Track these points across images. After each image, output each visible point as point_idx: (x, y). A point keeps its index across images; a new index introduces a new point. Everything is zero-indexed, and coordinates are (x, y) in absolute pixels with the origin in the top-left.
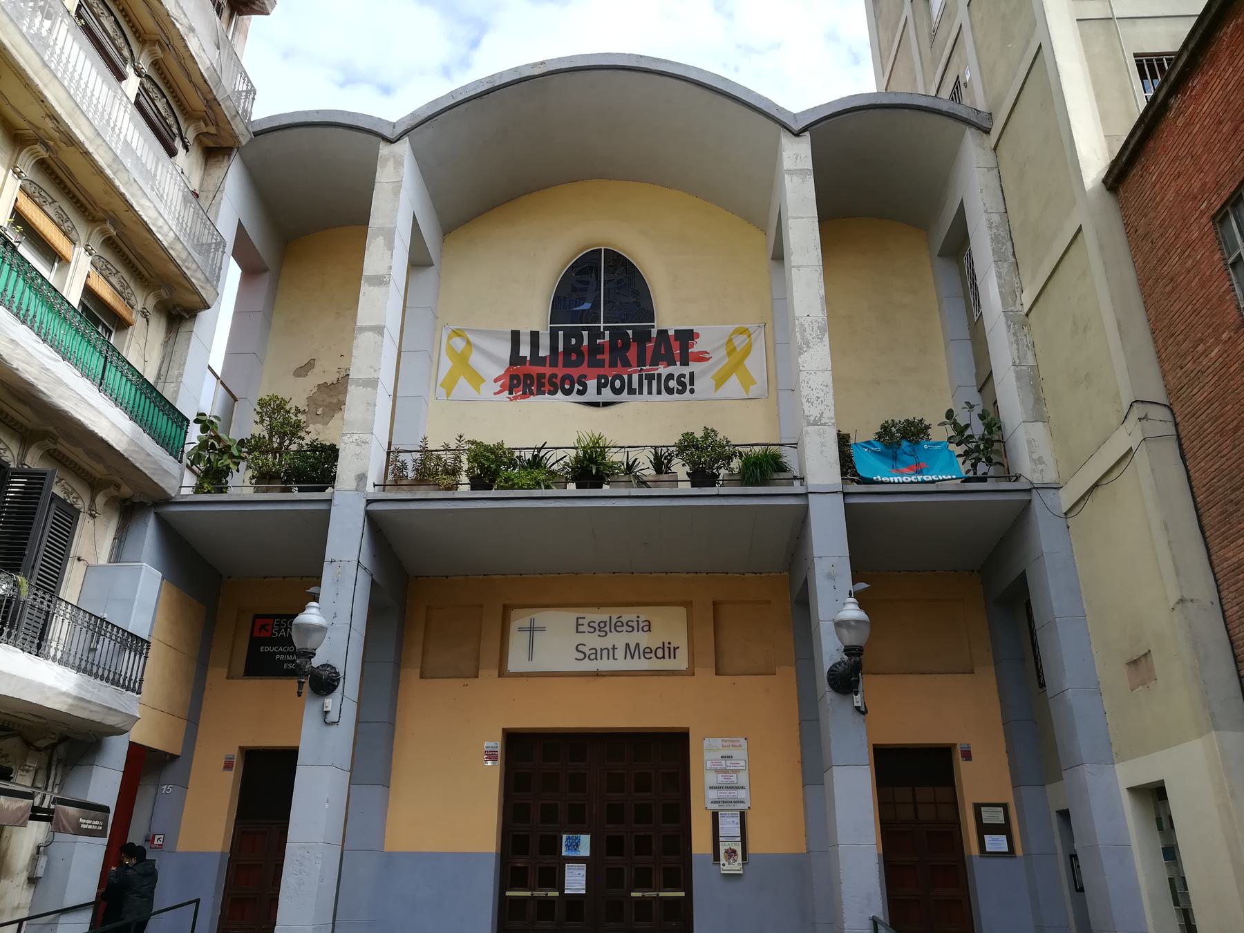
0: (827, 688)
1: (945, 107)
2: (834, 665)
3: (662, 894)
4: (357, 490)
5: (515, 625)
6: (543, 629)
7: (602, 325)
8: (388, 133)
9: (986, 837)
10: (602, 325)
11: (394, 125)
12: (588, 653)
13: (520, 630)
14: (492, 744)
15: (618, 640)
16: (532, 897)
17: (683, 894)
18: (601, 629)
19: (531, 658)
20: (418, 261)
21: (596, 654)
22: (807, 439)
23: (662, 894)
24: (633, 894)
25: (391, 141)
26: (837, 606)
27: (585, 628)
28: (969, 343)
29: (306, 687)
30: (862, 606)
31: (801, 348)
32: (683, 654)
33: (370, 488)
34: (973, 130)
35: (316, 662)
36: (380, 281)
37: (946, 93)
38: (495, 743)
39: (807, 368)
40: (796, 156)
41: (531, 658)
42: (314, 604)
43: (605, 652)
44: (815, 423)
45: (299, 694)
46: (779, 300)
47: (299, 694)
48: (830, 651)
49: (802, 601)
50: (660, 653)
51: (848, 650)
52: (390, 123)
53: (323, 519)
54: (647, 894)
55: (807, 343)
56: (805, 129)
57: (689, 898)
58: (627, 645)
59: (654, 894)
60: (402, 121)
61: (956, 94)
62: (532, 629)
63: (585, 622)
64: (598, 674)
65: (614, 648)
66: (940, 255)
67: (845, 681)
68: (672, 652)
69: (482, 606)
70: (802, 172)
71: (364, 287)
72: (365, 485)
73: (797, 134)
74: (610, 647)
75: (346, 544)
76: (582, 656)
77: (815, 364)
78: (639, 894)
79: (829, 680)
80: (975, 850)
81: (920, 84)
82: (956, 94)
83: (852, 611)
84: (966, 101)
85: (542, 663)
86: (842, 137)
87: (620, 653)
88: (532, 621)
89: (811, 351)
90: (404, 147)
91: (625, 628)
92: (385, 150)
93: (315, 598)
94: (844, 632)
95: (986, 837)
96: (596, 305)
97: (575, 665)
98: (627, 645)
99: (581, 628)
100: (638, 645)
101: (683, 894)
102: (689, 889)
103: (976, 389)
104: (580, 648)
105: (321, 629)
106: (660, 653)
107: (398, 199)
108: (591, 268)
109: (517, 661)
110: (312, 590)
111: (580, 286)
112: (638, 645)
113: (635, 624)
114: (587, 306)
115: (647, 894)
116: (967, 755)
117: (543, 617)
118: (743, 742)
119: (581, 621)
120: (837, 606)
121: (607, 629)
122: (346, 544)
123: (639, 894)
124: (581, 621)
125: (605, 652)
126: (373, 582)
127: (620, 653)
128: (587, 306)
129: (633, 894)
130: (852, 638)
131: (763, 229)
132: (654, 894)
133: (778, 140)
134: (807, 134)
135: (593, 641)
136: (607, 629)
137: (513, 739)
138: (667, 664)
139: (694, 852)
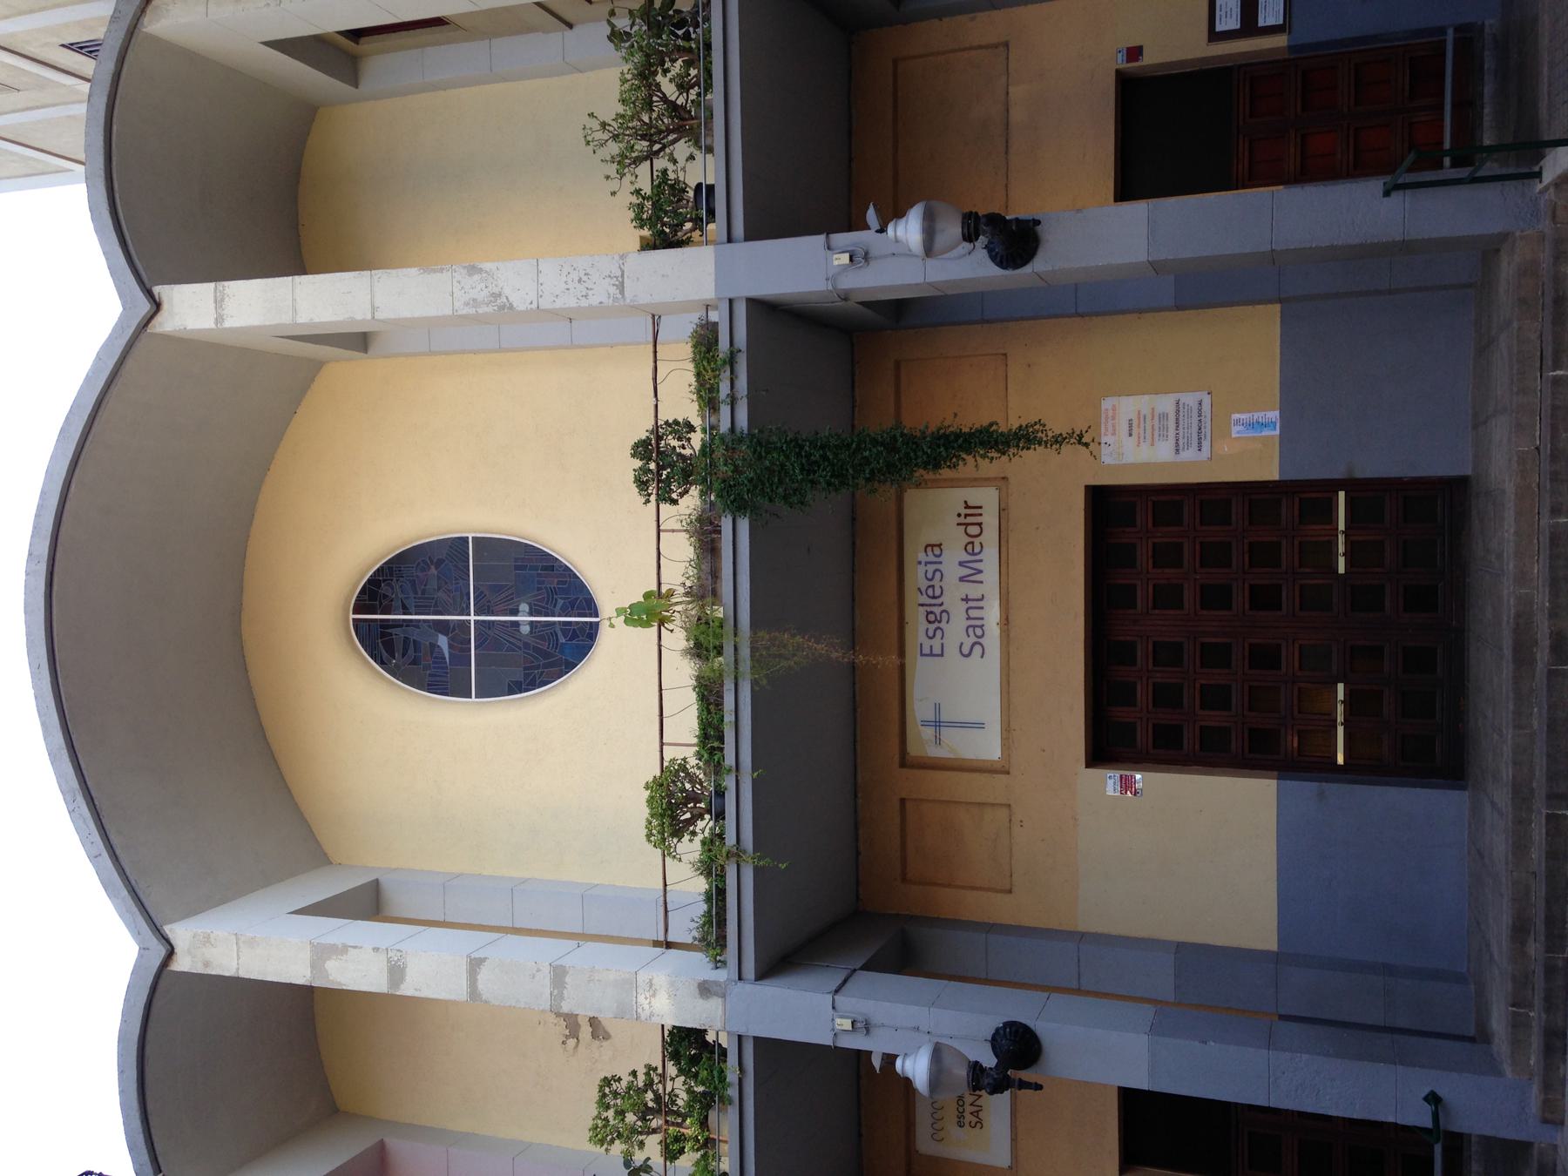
0: (1027, 269)
1: (110, 66)
2: (993, 258)
3: (1342, 526)
4: (724, 996)
5: (934, 752)
6: (937, 708)
7: (473, 618)
8: (160, 951)
9: (1261, 23)
10: (473, 618)
11: (143, 949)
12: (973, 639)
13: (938, 740)
14: (1110, 782)
15: (952, 598)
16: (1346, 724)
17: (1342, 495)
18: (936, 619)
19: (980, 726)
20: (368, 903)
21: (976, 627)
22: (644, 299)
23: (1342, 526)
24: (1341, 570)
25: (171, 953)
26: (903, 253)
27: (936, 643)
28: (496, 42)
29: (1027, 1075)
30: (899, 213)
31: (502, 308)
32: (975, 495)
33: (721, 975)
34: (146, 20)
35: (989, 1060)
36: (396, 972)
37: (86, 65)
38: (1109, 780)
39: (533, 296)
40: (192, 308)
41: (980, 726)
42: (899, 1063)
43: (973, 613)
44: (621, 287)
45: (1038, 1087)
46: (435, 341)
47: (1038, 1087)
48: (970, 266)
49: (899, 315)
50: (974, 530)
51: (969, 237)
52: (140, 956)
53: (771, 1052)
54: (1341, 549)
55: (497, 296)
56: (149, 294)
57: (1353, 486)
58: (962, 579)
59: (1341, 539)
60: (136, 934)
61: (87, 49)
62: (938, 724)
63: (927, 644)
64: (1006, 622)
65: (966, 600)
66: (354, 81)
67: (1015, 241)
68: (972, 509)
69: (903, 801)
70: (219, 302)
71: (406, 990)
72: (716, 983)
73: (157, 306)
74: (964, 605)
75: (807, 1011)
76: (978, 649)
77: (524, 278)
78: (1342, 561)
79: (1016, 267)
80: (1281, 41)
81: (70, 109)
82: (87, 49)
83: (909, 230)
84: (99, 33)
85: (989, 708)
86: (156, 228)
87: (973, 591)
88: (925, 723)
89: (507, 291)
90: (180, 933)
91: (936, 582)
92: (182, 964)
93: (890, 1059)
94: (940, 241)
95: (1261, 23)
96: (443, 627)
97: (991, 659)
98: (962, 579)
99: (937, 650)
100: (961, 564)
101: (1342, 495)
102: (1333, 486)
103: (568, 33)
104: (966, 650)
105: (937, 1054)
106: (974, 530)
107: (259, 942)
108: (383, 635)
109: (988, 747)
110: (876, 1062)
111: (411, 651)
112: (961, 564)
113: (931, 568)
114: (443, 641)
115: (1341, 549)
116: (1134, 53)
117: (920, 709)
118: (1107, 404)
119: (926, 650)
120: (903, 253)
121: (937, 610)
122: (807, 1011)
123: (1342, 561)
124: (926, 650)
125: (973, 613)
126: (867, 967)
127: (973, 591)
128: (443, 641)
129: (1341, 570)
130: (951, 229)
131: (317, 366)
132: (1341, 539)
133: (168, 338)
134: (157, 290)
135: (955, 630)
136: (937, 610)
137: (1107, 745)
138: (990, 519)
139: (1277, 478)
